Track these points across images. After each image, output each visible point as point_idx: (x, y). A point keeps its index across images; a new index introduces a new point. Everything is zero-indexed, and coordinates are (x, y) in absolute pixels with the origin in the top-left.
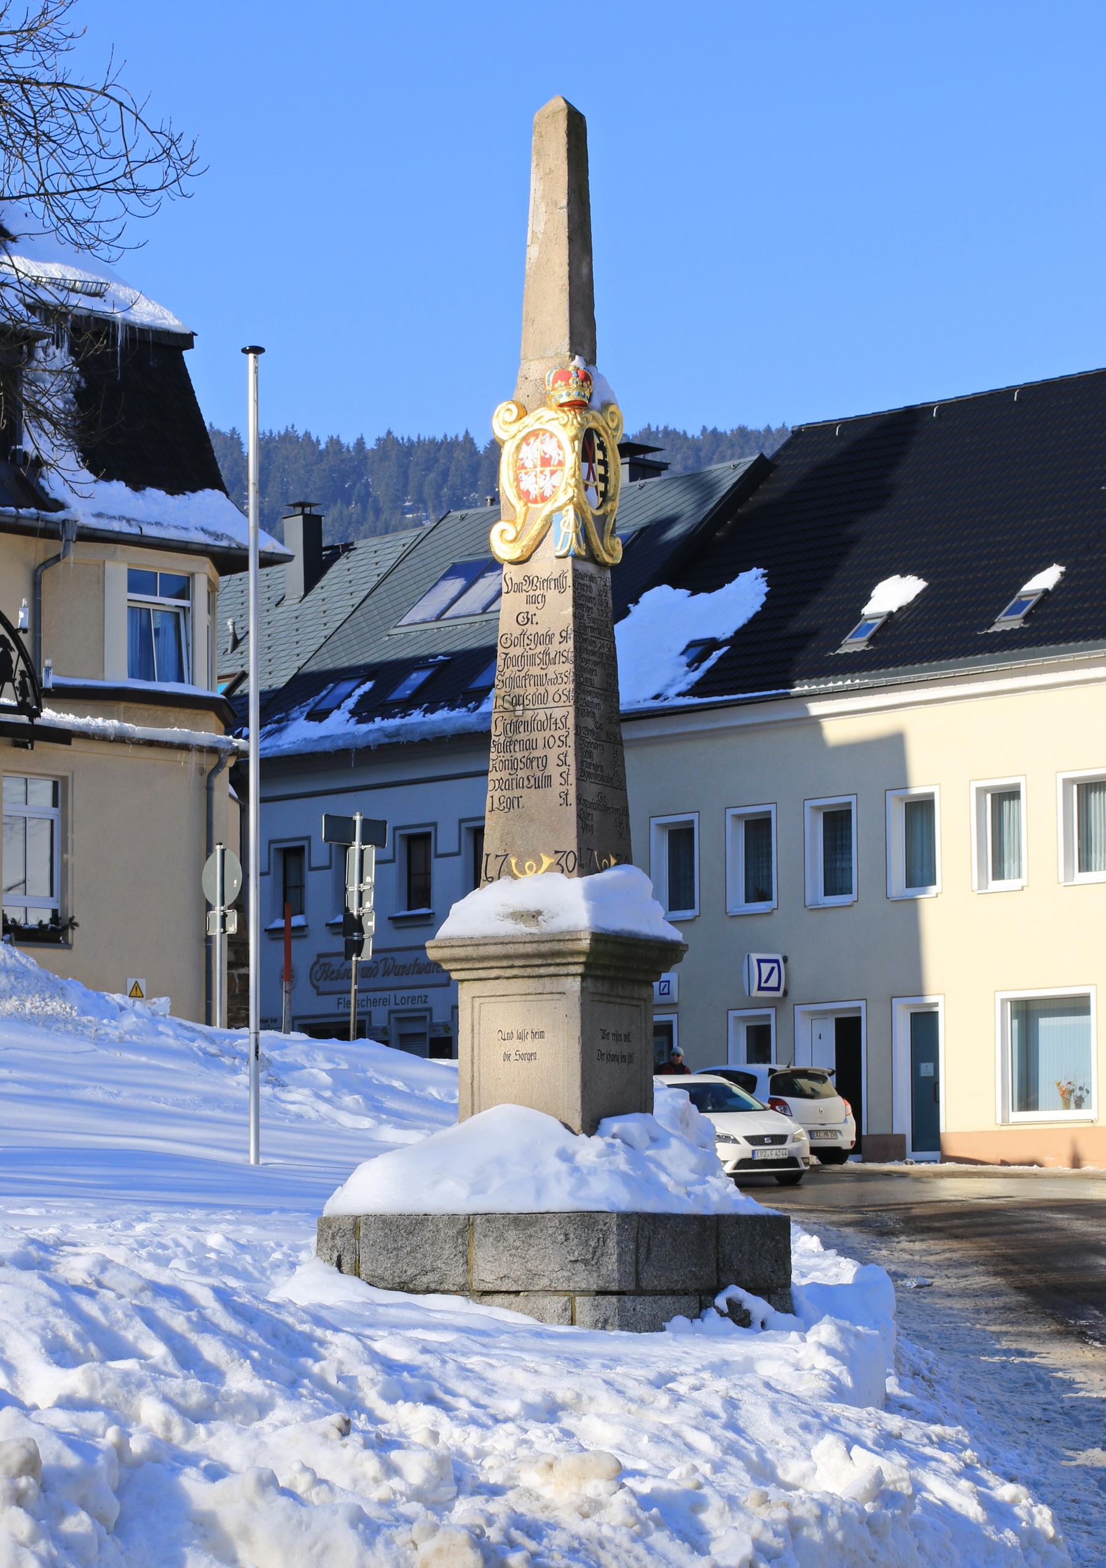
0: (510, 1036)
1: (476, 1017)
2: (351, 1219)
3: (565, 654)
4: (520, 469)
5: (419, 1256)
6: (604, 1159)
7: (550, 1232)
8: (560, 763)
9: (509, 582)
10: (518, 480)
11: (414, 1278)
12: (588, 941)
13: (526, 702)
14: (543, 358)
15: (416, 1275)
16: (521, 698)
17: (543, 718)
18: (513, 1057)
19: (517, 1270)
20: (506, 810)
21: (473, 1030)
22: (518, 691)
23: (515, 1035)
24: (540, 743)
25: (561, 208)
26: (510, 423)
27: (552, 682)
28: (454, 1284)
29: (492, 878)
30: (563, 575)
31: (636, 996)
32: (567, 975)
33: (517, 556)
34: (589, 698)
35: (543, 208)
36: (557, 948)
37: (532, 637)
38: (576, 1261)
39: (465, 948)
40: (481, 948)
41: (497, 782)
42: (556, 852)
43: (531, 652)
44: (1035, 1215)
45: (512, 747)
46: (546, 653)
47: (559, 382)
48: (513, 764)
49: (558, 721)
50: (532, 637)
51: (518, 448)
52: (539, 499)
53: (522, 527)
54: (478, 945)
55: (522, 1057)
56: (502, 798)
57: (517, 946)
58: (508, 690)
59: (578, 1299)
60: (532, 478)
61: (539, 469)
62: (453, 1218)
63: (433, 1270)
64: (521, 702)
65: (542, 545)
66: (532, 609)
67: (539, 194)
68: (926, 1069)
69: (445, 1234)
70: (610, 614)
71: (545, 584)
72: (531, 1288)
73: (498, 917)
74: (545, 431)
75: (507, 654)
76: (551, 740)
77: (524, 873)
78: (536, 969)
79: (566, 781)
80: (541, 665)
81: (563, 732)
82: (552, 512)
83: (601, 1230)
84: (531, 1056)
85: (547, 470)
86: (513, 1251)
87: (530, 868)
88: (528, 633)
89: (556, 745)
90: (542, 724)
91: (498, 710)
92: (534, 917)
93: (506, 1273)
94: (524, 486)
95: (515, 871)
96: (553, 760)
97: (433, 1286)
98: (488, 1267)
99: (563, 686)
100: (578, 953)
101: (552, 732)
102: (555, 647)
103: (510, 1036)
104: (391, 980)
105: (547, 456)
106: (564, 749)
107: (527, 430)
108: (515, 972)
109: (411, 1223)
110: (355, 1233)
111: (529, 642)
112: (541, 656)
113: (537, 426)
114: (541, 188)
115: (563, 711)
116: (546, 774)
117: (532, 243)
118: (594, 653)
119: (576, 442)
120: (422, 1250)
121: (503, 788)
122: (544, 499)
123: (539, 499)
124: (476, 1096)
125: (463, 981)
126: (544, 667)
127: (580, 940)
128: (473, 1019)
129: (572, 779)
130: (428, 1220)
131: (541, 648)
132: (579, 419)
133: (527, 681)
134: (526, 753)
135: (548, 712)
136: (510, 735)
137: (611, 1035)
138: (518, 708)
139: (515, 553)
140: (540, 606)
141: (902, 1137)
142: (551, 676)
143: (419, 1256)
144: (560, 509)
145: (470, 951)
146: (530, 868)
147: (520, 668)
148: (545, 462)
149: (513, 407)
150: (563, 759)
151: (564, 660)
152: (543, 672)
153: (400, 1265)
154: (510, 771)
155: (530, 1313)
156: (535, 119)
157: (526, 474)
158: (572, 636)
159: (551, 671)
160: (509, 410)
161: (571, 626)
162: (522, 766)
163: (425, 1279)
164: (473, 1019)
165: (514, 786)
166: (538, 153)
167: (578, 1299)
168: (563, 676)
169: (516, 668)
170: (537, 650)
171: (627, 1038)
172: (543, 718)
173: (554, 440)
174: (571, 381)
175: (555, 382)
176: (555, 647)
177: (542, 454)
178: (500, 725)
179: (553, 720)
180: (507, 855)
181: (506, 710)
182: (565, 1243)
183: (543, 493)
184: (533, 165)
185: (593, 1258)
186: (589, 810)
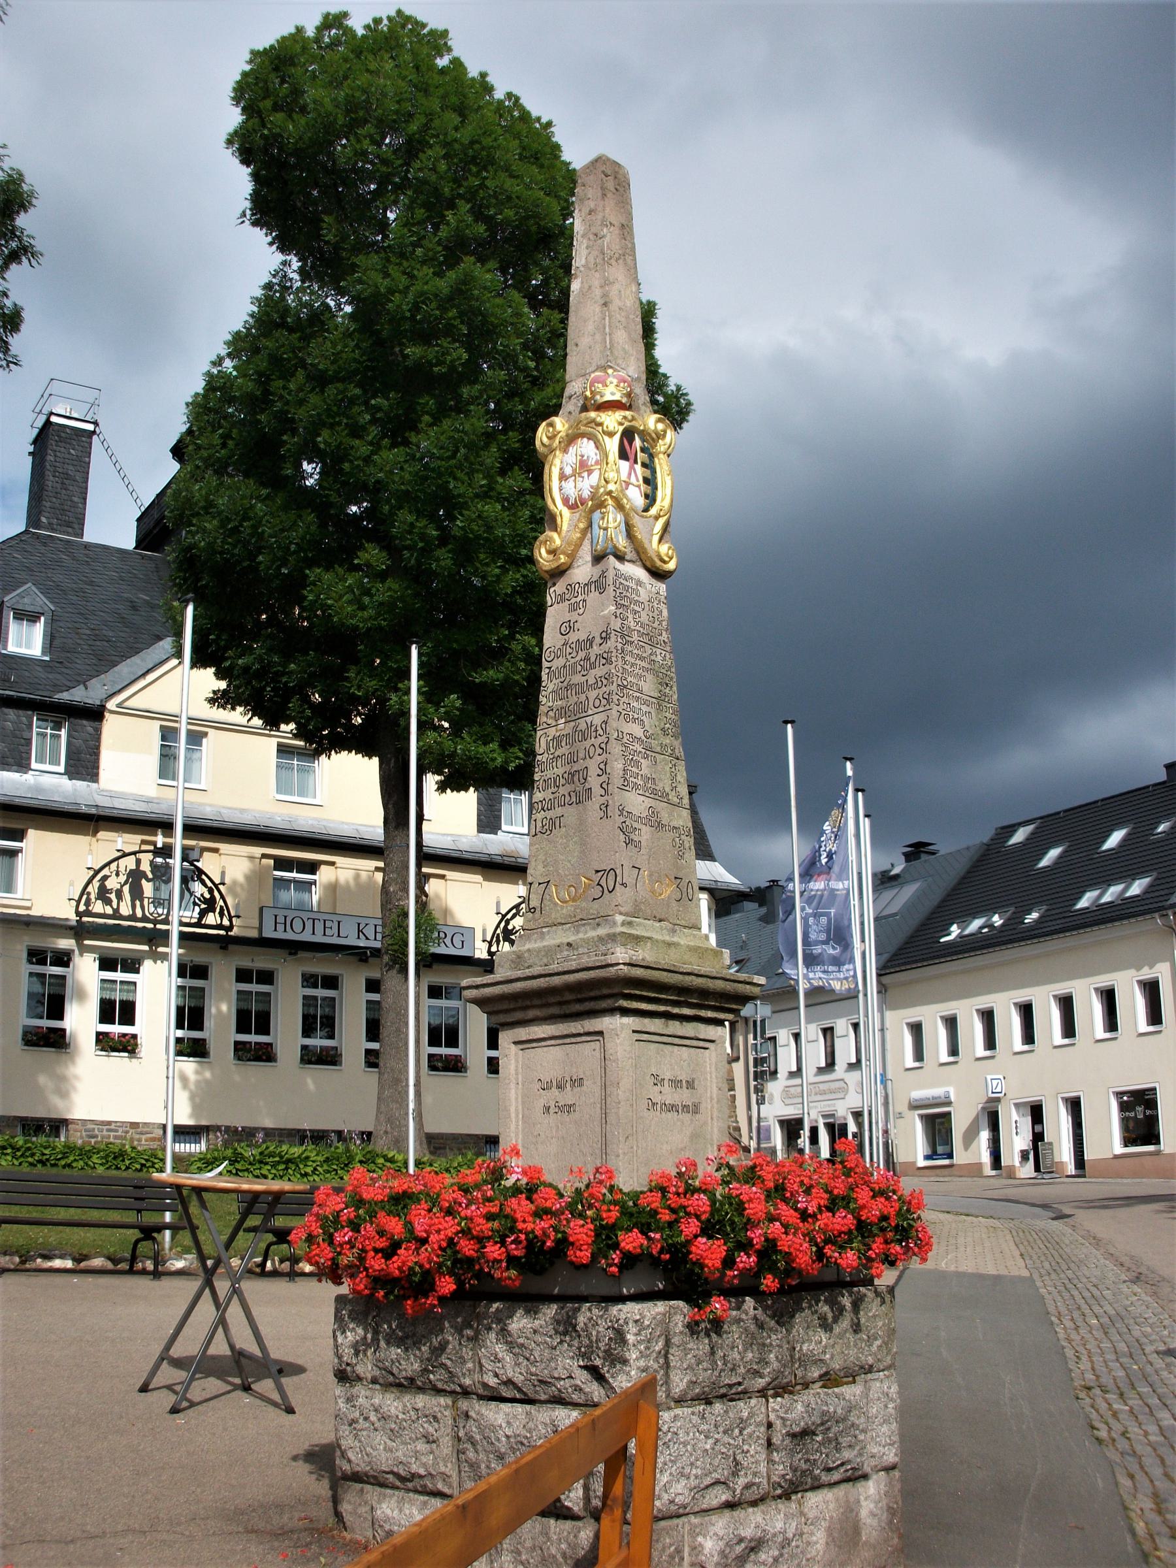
24: (581, 755)
27: (595, 686)
34: (635, 704)
42: (597, 871)
43: (573, 661)
46: (587, 659)
66: (574, 616)
70: (664, 623)
76: (592, 750)
84: (569, 1108)
96: (593, 771)
118: (642, 659)
135: (589, 719)
137: (666, 1082)
140: (581, 611)
170: (578, 658)
171: (690, 1085)
186: (635, 825)
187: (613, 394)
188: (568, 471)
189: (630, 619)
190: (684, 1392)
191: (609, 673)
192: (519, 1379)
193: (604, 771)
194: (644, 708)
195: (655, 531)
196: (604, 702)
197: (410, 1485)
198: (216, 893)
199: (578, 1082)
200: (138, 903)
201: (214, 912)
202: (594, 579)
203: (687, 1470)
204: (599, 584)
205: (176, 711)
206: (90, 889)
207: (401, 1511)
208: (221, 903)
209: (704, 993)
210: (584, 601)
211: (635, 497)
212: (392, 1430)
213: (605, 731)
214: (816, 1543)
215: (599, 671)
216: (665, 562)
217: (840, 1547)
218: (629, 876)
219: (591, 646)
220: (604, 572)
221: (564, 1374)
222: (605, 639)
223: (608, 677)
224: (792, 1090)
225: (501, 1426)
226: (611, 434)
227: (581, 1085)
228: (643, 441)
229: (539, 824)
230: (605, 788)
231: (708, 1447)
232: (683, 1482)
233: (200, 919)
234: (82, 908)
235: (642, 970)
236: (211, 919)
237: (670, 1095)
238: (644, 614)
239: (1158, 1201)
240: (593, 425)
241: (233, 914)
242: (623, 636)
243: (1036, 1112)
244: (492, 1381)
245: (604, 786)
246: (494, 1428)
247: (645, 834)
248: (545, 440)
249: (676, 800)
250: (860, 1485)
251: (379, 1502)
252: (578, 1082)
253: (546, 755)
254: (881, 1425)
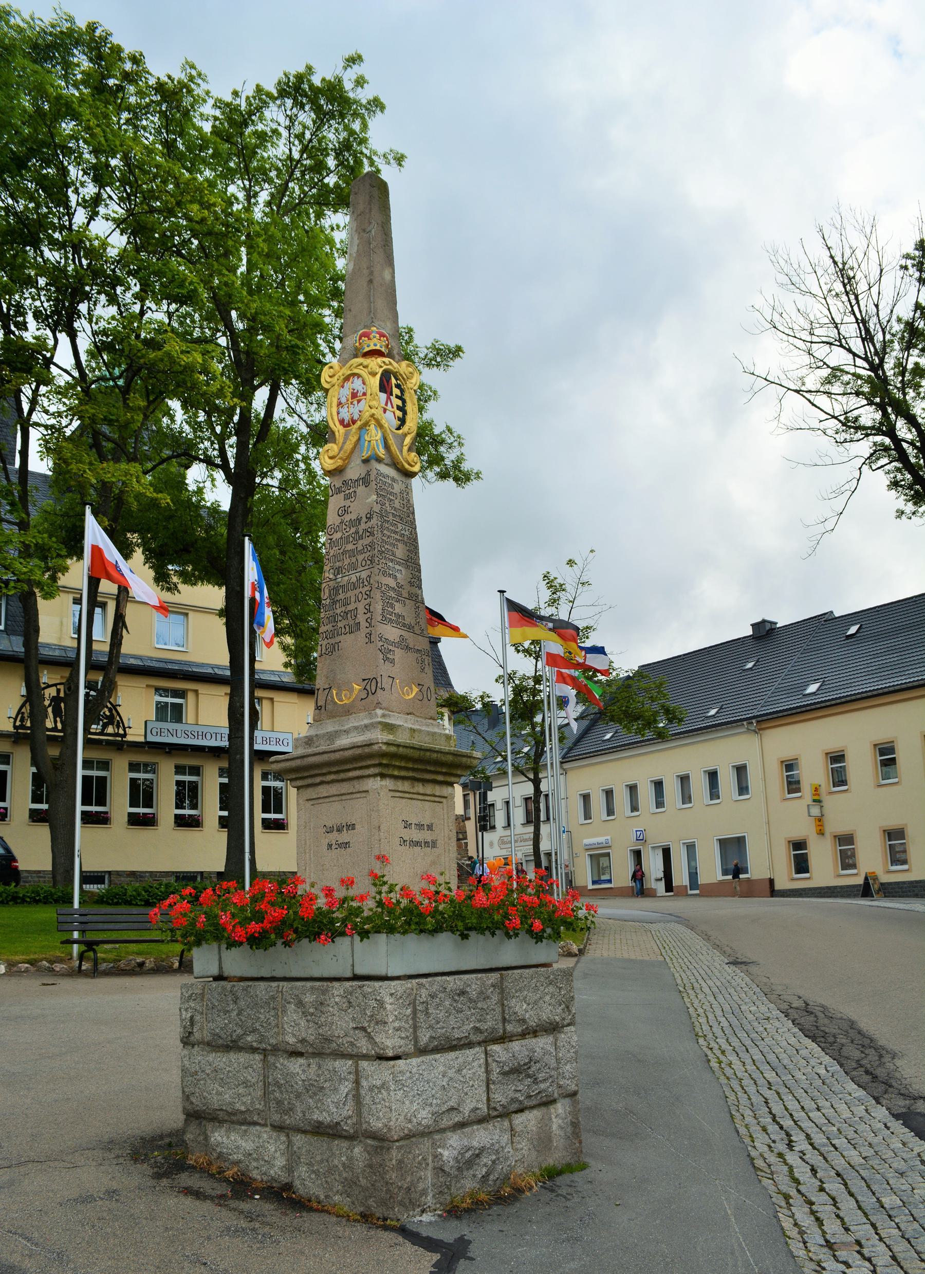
11: (240, 1037)
18: (333, 847)
24: (353, 599)
27: (361, 552)
31: (437, 794)
42: (364, 680)
43: (347, 534)
46: (357, 532)
66: (347, 503)
68: (693, 864)
84: (346, 845)
86: (309, 1018)
96: (361, 610)
104: (523, 844)
116: (357, 621)
118: (396, 533)
134: (343, 609)
141: (686, 886)
171: (430, 827)
178: (327, 591)
186: (390, 647)
187: (375, 345)
188: (343, 400)
189: (387, 505)
190: (427, 1045)
191: (372, 542)
192: (311, 1038)
193: (369, 611)
194: (397, 567)
195: (405, 443)
196: (368, 562)
197: (234, 1118)
198: (114, 712)
199: (351, 827)
200: (58, 719)
201: (113, 724)
203: (430, 1101)
204: (365, 480)
205: (80, 587)
206: (23, 710)
207: (228, 1138)
208: (118, 718)
209: (437, 763)
210: (355, 492)
211: (390, 419)
212: (222, 1079)
213: (369, 583)
214: (522, 1149)
215: (367, 541)
216: (412, 466)
217: (538, 1151)
218: (386, 682)
219: (360, 523)
220: (368, 472)
221: (342, 1034)
222: (369, 519)
223: (371, 545)
224: (505, 839)
225: (298, 1073)
226: (373, 374)
227: (354, 829)
228: (397, 379)
229: (324, 648)
230: (369, 621)
231: (444, 1083)
232: (428, 1109)
233: (103, 729)
234: (18, 723)
236: (110, 730)
237: (417, 835)
238: (397, 502)
240: (361, 367)
241: (126, 725)
242: (382, 516)
243: (666, 852)
244: (291, 1040)
246: (293, 1075)
247: (398, 654)
248: (329, 379)
249: (418, 632)
250: (552, 1109)
251: (213, 1132)
252: (351, 827)
253: (328, 601)
254: (566, 1064)
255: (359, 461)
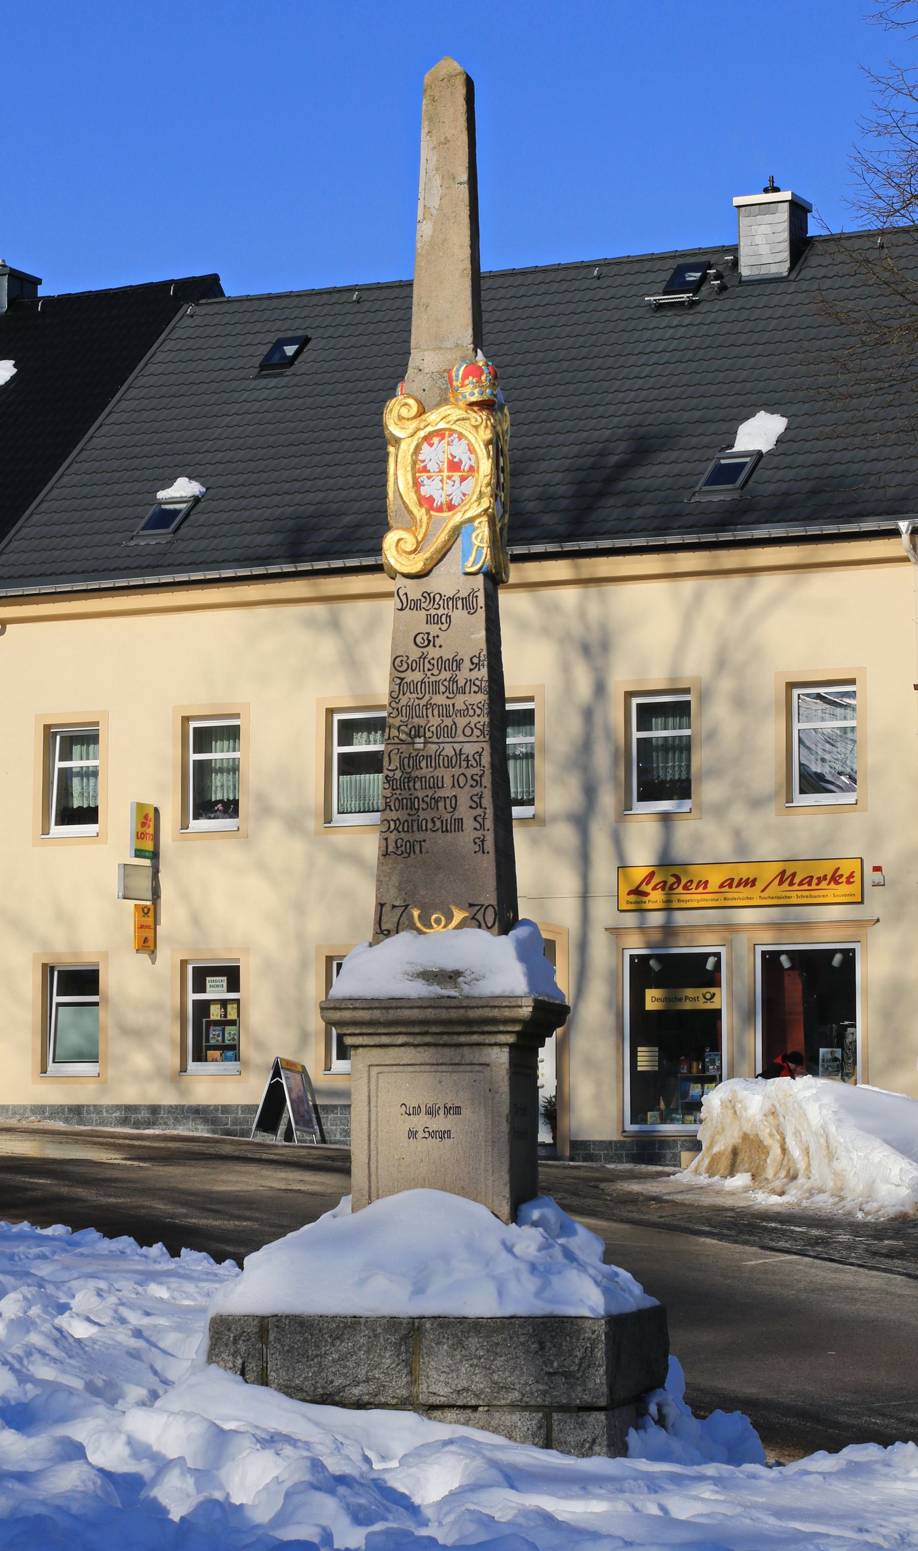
0: (416, 1111)
1: (373, 1087)
2: (258, 1320)
3: (477, 683)
4: (420, 472)
5: (350, 1364)
6: (544, 1252)
7: (522, 1339)
8: (474, 805)
9: (404, 598)
10: (417, 485)
11: (341, 1389)
12: (530, 1009)
13: (428, 734)
14: (440, 348)
15: (345, 1386)
16: (422, 730)
17: (451, 753)
18: (420, 1134)
19: (480, 1383)
20: (405, 855)
21: (369, 1103)
22: (422, 722)
23: (423, 1110)
24: (448, 782)
25: (461, 183)
26: (408, 419)
27: (463, 713)
28: (393, 1397)
29: (389, 931)
30: (473, 593)
32: (496, 1044)
33: (418, 570)
35: (437, 181)
36: (490, 1015)
37: (435, 662)
38: (554, 1374)
39: (370, 1012)
40: (391, 1011)
41: (392, 824)
42: (471, 905)
43: (433, 679)
44: (71, 1168)
45: (411, 784)
47: (471, 378)
48: (413, 804)
49: (470, 758)
50: (435, 662)
51: (418, 448)
52: (445, 507)
53: (423, 538)
54: (387, 1008)
55: (432, 1134)
56: (399, 841)
57: (438, 1011)
58: (405, 719)
59: (555, 1416)
60: (436, 483)
61: (445, 473)
62: (393, 1323)
63: (367, 1380)
64: (422, 733)
65: (445, 559)
66: (434, 630)
67: (432, 164)
69: (386, 1340)
71: (450, 603)
72: (495, 1402)
73: (407, 976)
74: (452, 431)
75: (402, 679)
76: (462, 779)
77: (430, 926)
78: (456, 1037)
79: (482, 826)
80: (447, 694)
81: (477, 770)
82: (462, 523)
83: (589, 1339)
84: (444, 1135)
85: (456, 476)
86: (475, 1361)
87: (438, 921)
88: (430, 657)
89: (468, 784)
90: (450, 760)
91: (393, 741)
92: (450, 977)
93: (466, 1385)
94: (425, 491)
95: (418, 925)
97: (366, 1398)
98: (442, 1378)
99: (475, 719)
100: (514, 1021)
101: (463, 770)
102: (464, 675)
103: (416, 1111)
105: (456, 460)
106: (477, 790)
107: (430, 429)
108: (428, 1039)
109: (338, 1326)
110: (261, 1337)
111: (431, 667)
112: (446, 683)
113: (442, 425)
114: (435, 158)
115: (476, 747)
117: (424, 218)
119: (491, 447)
120: (354, 1358)
121: (400, 829)
122: (451, 507)
123: (445, 507)
124: (373, 1177)
125: (356, 1047)
126: (451, 696)
127: (521, 1007)
128: (369, 1090)
129: (489, 824)
130: (359, 1323)
131: (445, 675)
132: (492, 421)
133: (430, 711)
136: (408, 770)
138: (417, 740)
139: (415, 565)
140: (444, 627)
142: (460, 706)
143: (350, 1364)
144: (471, 520)
145: (377, 1014)
146: (438, 921)
147: (420, 696)
148: (454, 466)
149: (411, 402)
150: (478, 801)
151: (476, 689)
152: (450, 702)
153: (324, 1375)
154: (408, 811)
155: (496, 1431)
156: (426, 80)
157: (429, 478)
158: (486, 663)
159: (460, 701)
160: (406, 404)
161: (485, 652)
162: (425, 806)
163: (356, 1391)
164: (369, 1090)
165: (415, 828)
166: (430, 119)
167: (555, 1416)
168: (475, 707)
169: (415, 695)
172: (451, 753)
173: (464, 442)
174: (483, 378)
175: (465, 377)
176: (464, 675)
177: (450, 457)
179: (463, 757)
180: (407, 906)
181: (403, 742)
182: (540, 1353)
183: (451, 500)
184: (424, 132)
185: (578, 1370)
202: (461, 595)
219: (458, 667)
235: (487, 1041)
239: (177, 1141)
245: (479, 819)
255: (457, 570)
